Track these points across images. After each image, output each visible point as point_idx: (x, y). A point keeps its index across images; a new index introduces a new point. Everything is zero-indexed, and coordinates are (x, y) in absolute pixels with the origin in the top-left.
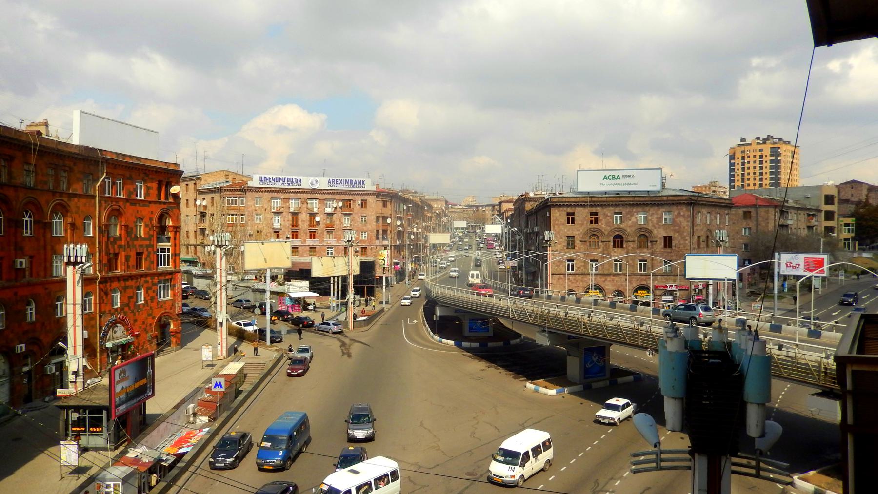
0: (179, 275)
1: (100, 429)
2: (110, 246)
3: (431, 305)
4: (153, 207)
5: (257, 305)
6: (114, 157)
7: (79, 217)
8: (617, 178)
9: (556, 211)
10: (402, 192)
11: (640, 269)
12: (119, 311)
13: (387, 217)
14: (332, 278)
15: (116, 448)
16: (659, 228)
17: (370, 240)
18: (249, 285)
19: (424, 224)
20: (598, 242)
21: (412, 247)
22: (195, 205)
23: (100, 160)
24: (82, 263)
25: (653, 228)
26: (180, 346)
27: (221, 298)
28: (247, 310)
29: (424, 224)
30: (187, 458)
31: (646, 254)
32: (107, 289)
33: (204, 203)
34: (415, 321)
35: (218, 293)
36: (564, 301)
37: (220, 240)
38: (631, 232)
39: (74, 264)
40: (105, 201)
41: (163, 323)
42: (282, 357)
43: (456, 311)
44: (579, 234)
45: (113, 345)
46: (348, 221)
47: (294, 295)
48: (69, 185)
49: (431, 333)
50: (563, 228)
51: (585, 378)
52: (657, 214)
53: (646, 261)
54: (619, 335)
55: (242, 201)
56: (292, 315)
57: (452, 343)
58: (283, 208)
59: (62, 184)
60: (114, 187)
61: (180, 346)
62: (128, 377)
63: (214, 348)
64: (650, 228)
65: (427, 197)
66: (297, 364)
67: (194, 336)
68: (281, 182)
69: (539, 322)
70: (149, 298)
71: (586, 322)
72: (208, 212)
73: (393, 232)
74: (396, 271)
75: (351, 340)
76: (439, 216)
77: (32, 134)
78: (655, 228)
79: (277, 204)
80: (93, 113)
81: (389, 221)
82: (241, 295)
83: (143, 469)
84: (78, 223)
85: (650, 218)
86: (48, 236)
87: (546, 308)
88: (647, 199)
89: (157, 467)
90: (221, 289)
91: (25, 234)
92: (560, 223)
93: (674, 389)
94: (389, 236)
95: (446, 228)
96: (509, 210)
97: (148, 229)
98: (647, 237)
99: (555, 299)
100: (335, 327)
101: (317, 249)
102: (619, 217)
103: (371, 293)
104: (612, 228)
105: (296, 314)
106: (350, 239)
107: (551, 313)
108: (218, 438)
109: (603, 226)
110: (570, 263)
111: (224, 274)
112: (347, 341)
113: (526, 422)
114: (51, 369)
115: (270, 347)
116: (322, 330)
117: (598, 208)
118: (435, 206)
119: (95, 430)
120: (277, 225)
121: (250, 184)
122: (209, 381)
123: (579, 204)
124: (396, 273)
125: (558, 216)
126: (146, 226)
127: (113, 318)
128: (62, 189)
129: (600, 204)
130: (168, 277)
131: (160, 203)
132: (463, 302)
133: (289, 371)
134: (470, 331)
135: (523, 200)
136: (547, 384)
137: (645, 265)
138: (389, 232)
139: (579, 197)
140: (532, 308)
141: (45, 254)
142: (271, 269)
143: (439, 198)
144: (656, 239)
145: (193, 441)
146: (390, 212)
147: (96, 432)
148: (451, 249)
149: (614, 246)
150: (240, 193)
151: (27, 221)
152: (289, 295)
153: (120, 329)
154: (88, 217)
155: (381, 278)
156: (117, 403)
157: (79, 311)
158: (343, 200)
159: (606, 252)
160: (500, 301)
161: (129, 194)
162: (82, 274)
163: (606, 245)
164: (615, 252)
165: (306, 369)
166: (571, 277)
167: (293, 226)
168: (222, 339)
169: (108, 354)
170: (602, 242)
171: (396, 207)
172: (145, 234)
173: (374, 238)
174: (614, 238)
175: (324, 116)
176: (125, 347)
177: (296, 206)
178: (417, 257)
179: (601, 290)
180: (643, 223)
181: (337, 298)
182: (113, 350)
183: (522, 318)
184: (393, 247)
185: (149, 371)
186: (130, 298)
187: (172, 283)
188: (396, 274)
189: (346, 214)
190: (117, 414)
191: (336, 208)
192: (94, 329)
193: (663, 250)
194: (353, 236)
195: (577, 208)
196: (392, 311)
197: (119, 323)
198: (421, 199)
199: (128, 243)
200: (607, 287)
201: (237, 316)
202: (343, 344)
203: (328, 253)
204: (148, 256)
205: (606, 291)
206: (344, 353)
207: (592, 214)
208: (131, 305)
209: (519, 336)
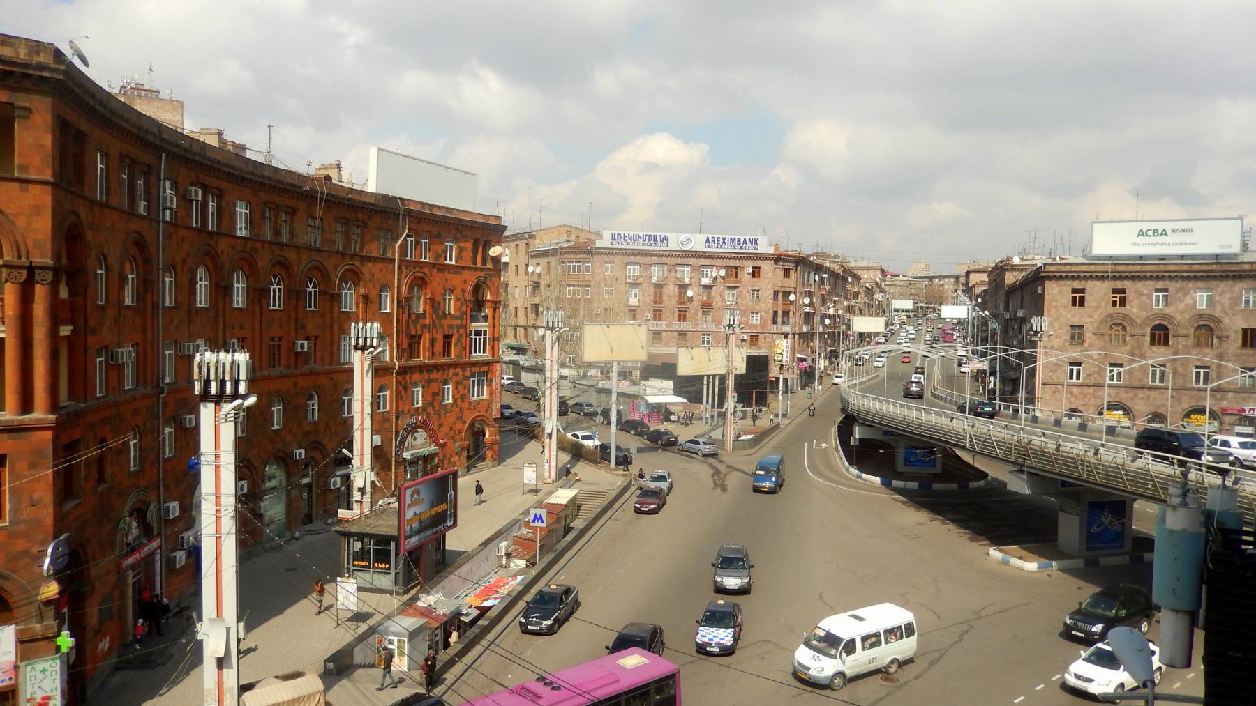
0: (498, 367)
1: (387, 566)
2: (412, 326)
3: (849, 421)
4: (466, 274)
5: (599, 412)
6: (419, 208)
7: (374, 287)
8: (1162, 234)
9: (1054, 285)
10: (817, 256)
11: (1198, 381)
12: (420, 411)
13: (790, 293)
14: (705, 378)
15: (405, 593)
16: (1234, 315)
17: (764, 325)
18: (592, 383)
19: (846, 303)
20: (1124, 335)
21: (826, 336)
22: (527, 273)
23: (401, 213)
24: (372, 346)
25: (1222, 315)
26: (497, 462)
27: (551, 400)
28: (588, 418)
29: (846, 303)
30: (492, 614)
31: (1209, 357)
32: (406, 382)
33: (538, 270)
34: (824, 445)
35: (548, 392)
36: (1060, 427)
37: (551, 320)
38: (1183, 321)
39: (363, 348)
40: (407, 266)
41: (476, 430)
42: (629, 485)
43: (885, 433)
44: (1091, 322)
45: (412, 455)
46: (733, 296)
47: (652, 400)
48: (362, 245)
49: (847, 464)
50: (1064, 313)
51: (1088, 549)
52: (1233, 292)
53: (1208, 368)
54: (1147, 484)
55: (588, 267)
56: (648, 427)
57: (877, 480)
58: (642, 277)
59: (353, 243)
60: (418, 247)
61: (497, 462)
62: (423, 499)
63: (540, 467)
64: (1217, 315)
65: (852, 264)
66: (649, 496)
67: (517, 449)
68: (641, 241)
69: (1013, 458)
70: (459, 396)
71: (1092, 461)
72: (543, 283)
73: (798, 314)
74: (801, 370)
75: (729, 467)
76: (869, 292)
77: (319, 179)
78: (1227, 314)
79: (634, 271)
80: (396, 151)
81: (792, 297)
82: (578, 396)
83: (435, 625)
84: (373, 294)
85: (1218, 298)
86: (336, 309)
87: (1025, 436)
88: (1214, 267)
89: (454, 622)
90: (551, 388)
91: (198, 305)
92: (1059, 304)
93: (1175, 594)
94: (791, 320)
95: (881, 310)
96: (982, 283)
97: (459, 303)
98: (1211, 329)
99: (1043, 423)
100: (707, 447)
101: (687, 336)
102: (1163, 296)
103: (762, 400)
104: (1150, 313)
105: (654, 427)
106: (732, 323)
107: (1034, 445)
108: (534, 591)
109: (1135, 310)
110: (1075, 368)
111: (555, 367)
112: (722, 468)
113: (984, 609)
114: (336, 482)
115: (614, 470)
116: (688, 451)
117: (1126, 282)
118: (865, 276)
119: (380, 566)
120: (633, 301)
121: (599, 244)
122: (527, 512)
123: (1094, 275)
124: (801, 373)
125: (1056, 294)
126: (457, 299)
127: (413, 420)
128: (353, 251)
129: (1130, 275)
130: (484, 369)
131: (476, 269)
132: (894, 421)
133: (637, 505)
134: (905, 465)
135: (1000, 270)
136: (1024, 553)
137: (1206, 374)
138: (791, 313)
139: (1093, 264)
140: (1002, 435)
141: (332, 335)
142: (619, 363)
143: (871, 265)
144: (1227, 333)
145: (504, 591)
146: (794, 285)
147: (382, 568)
148: (886, 340)
149: (1152, 343)
150: (585, 256)
151: (274, 290)
152: (645, 399)
153: (421, 435)
154: (386, 287)
155: (778, 379)
156: (408, 533)
157: (368, 410)
158: (726, 267)
159: (1137, 351)
160: (951, 421)
161: (437, 257)
162: (372, 362)
163: (1137, 342)
164: (1153, 352)
165: (661, 503)
166: (1075, 390)
167: (655, 302)
168: (553, 457)
169: (405, 467)
170: (1131, 336)
171: (804, 278)
172: (455, 310)
173: (769, 322)
174: (1152, 329)
175: (705, 147)
176: (427, 459)
177: (661, 275)
178: (835, 351)
179: (1127, 411)
180: (1204, 307)
181: (713, 406)
182: (413, 462)
183: (986, 449)
184: (797, 336)
185: (450, 493)
186: (435, 394)
187: (489, 377)
188: (801, 375)
189: (729, 287)
190: (407, 547)
191: (715, 278)
192: (389, 434)
193: (1239, 351)
194: (736, 319)
195: (1089, 282)
196: (790, 428)
197: (421, 427)
198: (842, 266)
199: (433, 321)
200: (1137, 408)
201: (575, 425)
202: (717, 472)
203: (703, 342)
204: (459, 340)
205: (1135, 413)
206: (716, 485)
207: (1115, 291)
208: (436, 404)
209: (984, 475)
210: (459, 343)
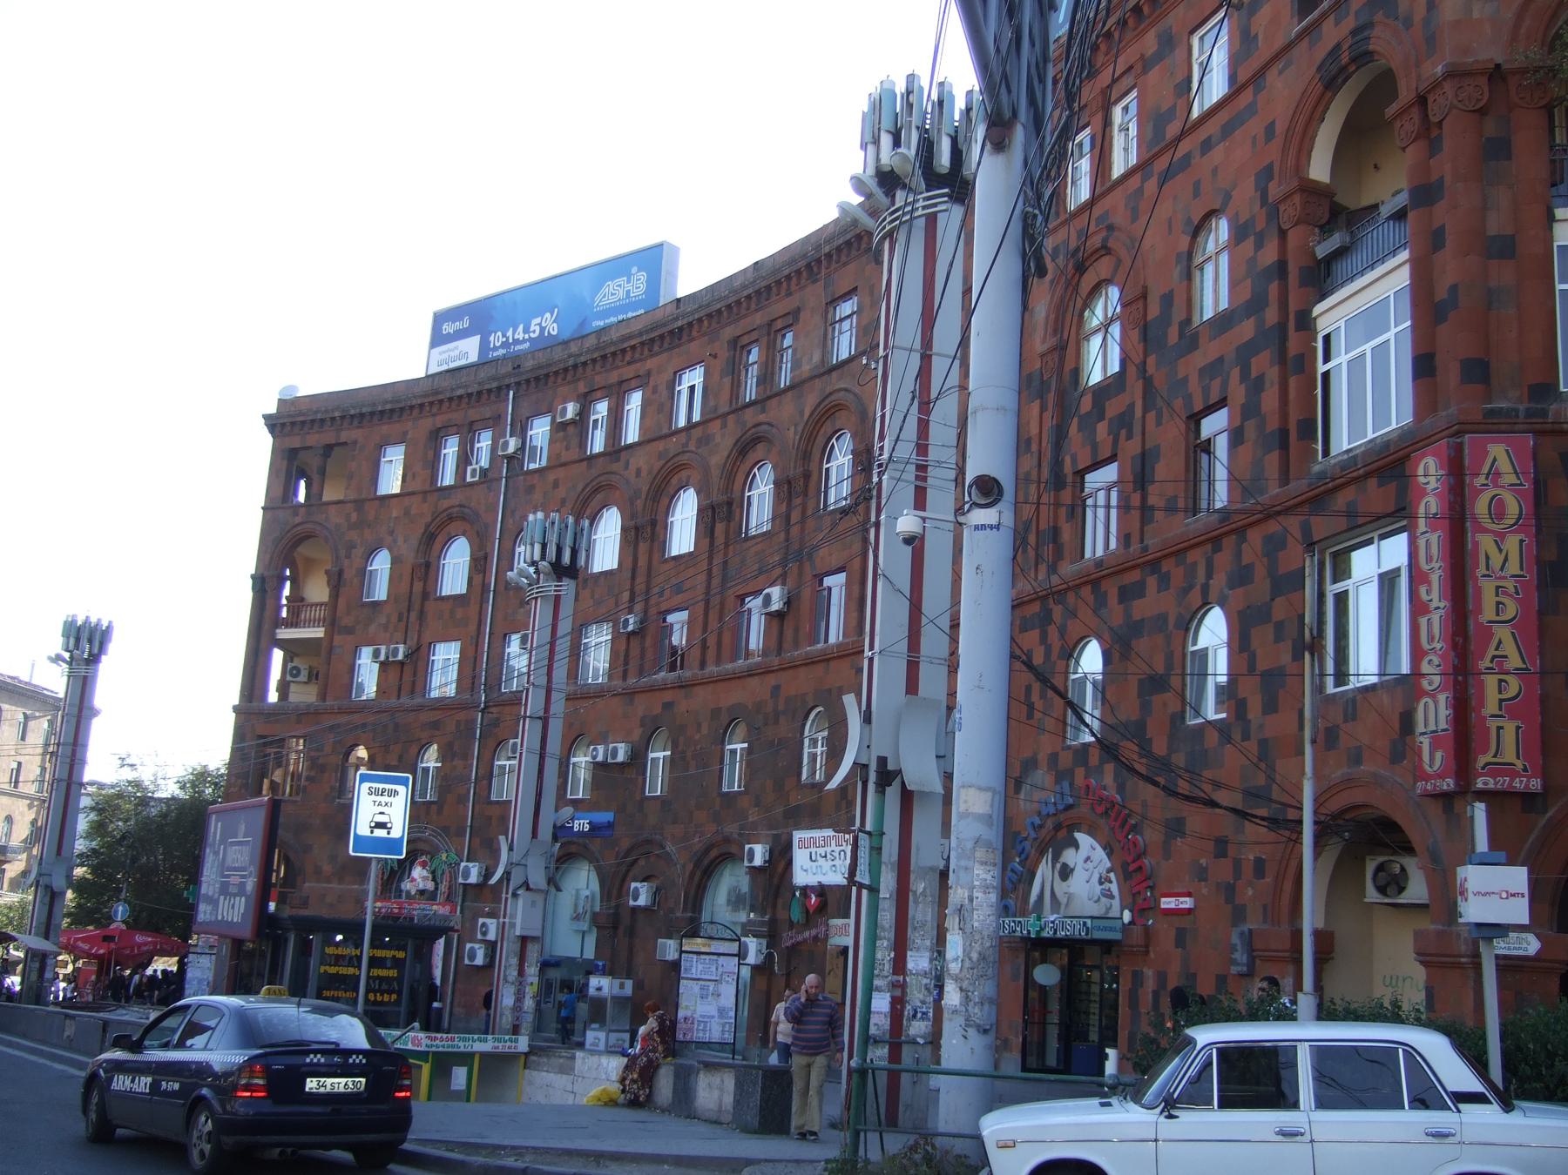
210: (1250, 426)
